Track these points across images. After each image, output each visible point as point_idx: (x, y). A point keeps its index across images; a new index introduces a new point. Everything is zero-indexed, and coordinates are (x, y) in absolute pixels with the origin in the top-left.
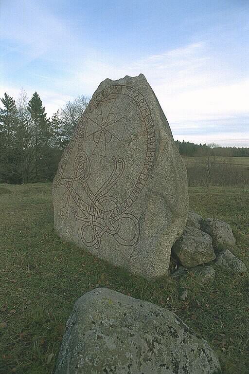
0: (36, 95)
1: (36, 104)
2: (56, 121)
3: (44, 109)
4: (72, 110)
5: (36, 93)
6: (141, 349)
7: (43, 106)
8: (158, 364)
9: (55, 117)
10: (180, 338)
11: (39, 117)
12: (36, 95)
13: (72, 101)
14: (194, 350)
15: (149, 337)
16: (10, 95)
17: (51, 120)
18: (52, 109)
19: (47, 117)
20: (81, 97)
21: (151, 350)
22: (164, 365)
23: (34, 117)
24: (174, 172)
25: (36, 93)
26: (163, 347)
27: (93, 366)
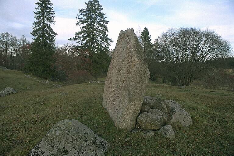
0: (146, 29)
1: (146, 33)
2: (157, 44)
3: (150, 37)
4: (165, 37)
5: (146, 27)
6: (68, 139)
7: (149, 35)
8: (72, 147)
9: (156, 41)
10: (87, 143)
11: (147, 41)
12: (146, 29)
13: (165, 32)
14: (51, 152)
15: (74, 137)
16: (149, 30)
17: (153, 43)
18: (154, 37)
19: (152, 42)
20: (170, 29)
21: (72, 141)
22: (75, 148)
23: (144, 41)
24: (136, 78)
25: (146, 27)
26: (78, 143)
27: (49, 137)
